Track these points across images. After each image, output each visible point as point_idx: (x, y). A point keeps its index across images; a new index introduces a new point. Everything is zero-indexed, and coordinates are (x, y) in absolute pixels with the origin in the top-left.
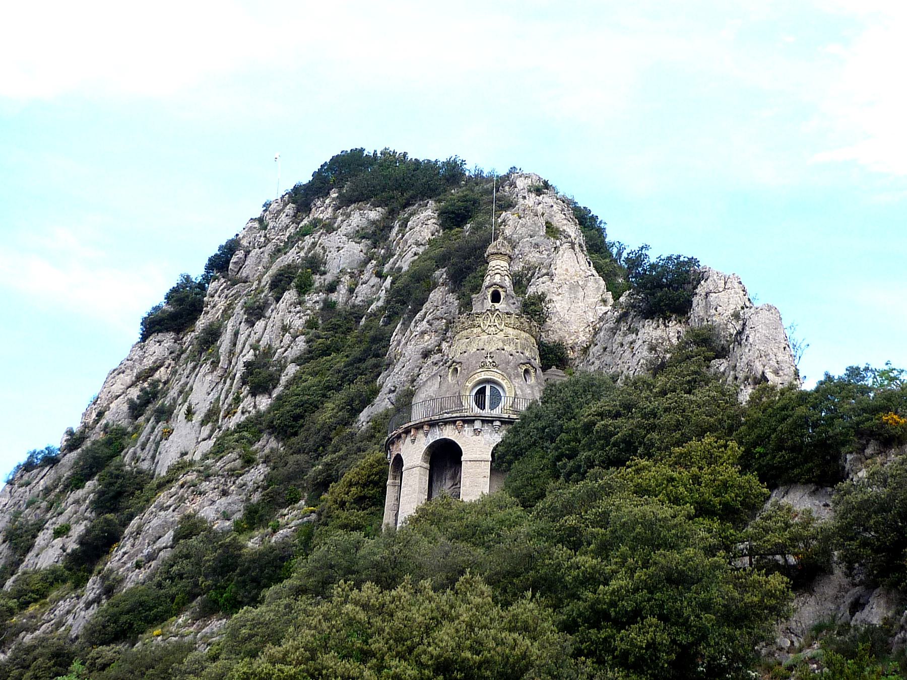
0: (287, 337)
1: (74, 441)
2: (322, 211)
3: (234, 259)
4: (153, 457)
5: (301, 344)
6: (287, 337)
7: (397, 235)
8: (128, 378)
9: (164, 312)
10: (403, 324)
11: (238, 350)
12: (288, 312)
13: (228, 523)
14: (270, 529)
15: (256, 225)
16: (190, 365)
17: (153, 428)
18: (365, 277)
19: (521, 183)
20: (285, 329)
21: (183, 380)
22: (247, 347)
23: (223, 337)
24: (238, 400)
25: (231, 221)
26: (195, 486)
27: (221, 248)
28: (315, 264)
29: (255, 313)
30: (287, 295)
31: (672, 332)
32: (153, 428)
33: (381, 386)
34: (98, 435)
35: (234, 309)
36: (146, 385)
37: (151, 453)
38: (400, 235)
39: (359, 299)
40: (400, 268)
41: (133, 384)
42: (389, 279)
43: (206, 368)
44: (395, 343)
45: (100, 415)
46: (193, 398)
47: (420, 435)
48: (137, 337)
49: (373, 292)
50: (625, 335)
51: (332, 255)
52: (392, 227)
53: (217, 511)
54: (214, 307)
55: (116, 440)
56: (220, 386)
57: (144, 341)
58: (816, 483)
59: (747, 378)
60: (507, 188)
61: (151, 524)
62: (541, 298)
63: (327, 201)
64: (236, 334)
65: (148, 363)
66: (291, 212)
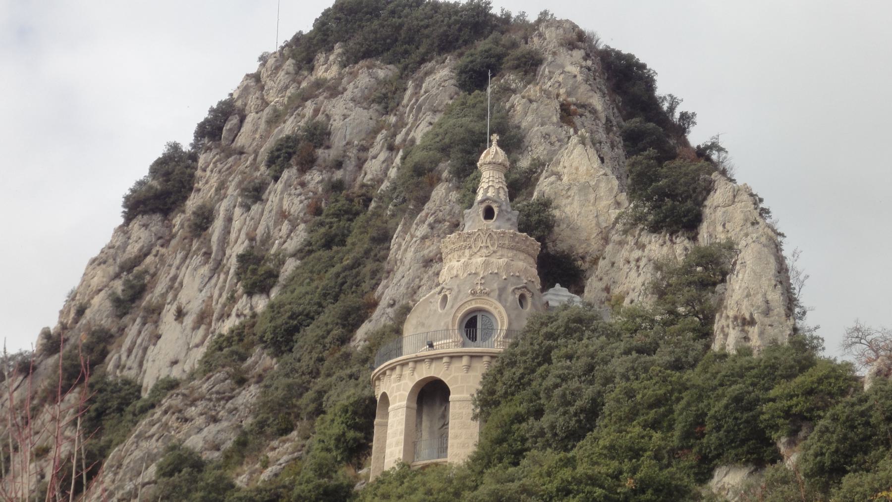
0: (285, 227)
1: (52, 343)
2: (327, 69)
3: (227, 127)
4: (141, 365)
5: (301, 235)
6: (285, 227)
7: (410, 100)
8: (112, 269)
9: (151, 187)
10: (405, 224)
11: (233, 236)
12: (287, 196)
13: (217, 454)
14: (258, 466)
15: (252, 83)
16: (180, 256)
17: (140, 332)
18: (372, 152)
19: (551, 34)
20: (283, 215)
21: (173, 271)
22: (243, 236)
23: (216, 221)
24: (233, 299)
25: (221, 78)
26: (180, 411)
27: (212, 111)
28: (318, 135)
29: (255, 193)
30: (285, 175)
31: (678, 249)
32: (140, 332)
33: (380, 298)
34: (80, 337)
35: (227, 188)
36: (131, 277)
37: (138, 360)
38: (413, 101)
39: (369, 176)
40: (413, 141)
41: (117, 276)
42: (401, 153)
43: (197, 260)
44: (396, 246)
45: (81, 312)
46: (183, 297)
47: (407, 371)
48: (121, 221)
49: (381, 168)
50: (632, 250)
51: (336, 123)
52: (405, 90)
53: (205, 440)
54: (207, 183)
55: (101, 343)
56: (213, 281)
57: (128, 225)
58: (755, 464)
59: (736, 318)
60: (535, 39)
61: (132, 457)
62: (546, 204)
63: (332, 58)
64: (229, 220)
65: (133, 249)
66: (291, 69)
